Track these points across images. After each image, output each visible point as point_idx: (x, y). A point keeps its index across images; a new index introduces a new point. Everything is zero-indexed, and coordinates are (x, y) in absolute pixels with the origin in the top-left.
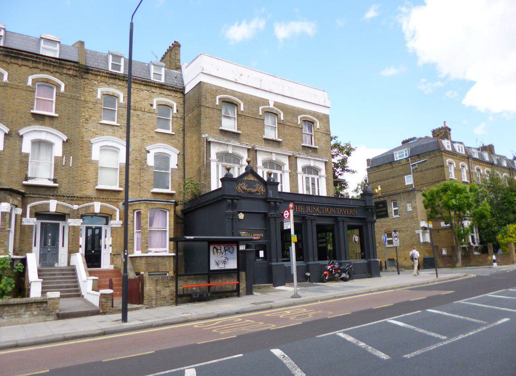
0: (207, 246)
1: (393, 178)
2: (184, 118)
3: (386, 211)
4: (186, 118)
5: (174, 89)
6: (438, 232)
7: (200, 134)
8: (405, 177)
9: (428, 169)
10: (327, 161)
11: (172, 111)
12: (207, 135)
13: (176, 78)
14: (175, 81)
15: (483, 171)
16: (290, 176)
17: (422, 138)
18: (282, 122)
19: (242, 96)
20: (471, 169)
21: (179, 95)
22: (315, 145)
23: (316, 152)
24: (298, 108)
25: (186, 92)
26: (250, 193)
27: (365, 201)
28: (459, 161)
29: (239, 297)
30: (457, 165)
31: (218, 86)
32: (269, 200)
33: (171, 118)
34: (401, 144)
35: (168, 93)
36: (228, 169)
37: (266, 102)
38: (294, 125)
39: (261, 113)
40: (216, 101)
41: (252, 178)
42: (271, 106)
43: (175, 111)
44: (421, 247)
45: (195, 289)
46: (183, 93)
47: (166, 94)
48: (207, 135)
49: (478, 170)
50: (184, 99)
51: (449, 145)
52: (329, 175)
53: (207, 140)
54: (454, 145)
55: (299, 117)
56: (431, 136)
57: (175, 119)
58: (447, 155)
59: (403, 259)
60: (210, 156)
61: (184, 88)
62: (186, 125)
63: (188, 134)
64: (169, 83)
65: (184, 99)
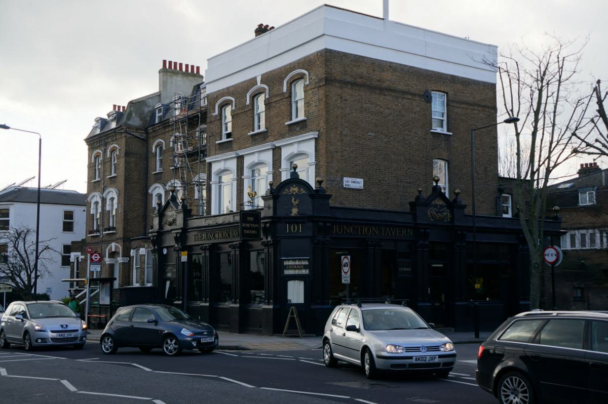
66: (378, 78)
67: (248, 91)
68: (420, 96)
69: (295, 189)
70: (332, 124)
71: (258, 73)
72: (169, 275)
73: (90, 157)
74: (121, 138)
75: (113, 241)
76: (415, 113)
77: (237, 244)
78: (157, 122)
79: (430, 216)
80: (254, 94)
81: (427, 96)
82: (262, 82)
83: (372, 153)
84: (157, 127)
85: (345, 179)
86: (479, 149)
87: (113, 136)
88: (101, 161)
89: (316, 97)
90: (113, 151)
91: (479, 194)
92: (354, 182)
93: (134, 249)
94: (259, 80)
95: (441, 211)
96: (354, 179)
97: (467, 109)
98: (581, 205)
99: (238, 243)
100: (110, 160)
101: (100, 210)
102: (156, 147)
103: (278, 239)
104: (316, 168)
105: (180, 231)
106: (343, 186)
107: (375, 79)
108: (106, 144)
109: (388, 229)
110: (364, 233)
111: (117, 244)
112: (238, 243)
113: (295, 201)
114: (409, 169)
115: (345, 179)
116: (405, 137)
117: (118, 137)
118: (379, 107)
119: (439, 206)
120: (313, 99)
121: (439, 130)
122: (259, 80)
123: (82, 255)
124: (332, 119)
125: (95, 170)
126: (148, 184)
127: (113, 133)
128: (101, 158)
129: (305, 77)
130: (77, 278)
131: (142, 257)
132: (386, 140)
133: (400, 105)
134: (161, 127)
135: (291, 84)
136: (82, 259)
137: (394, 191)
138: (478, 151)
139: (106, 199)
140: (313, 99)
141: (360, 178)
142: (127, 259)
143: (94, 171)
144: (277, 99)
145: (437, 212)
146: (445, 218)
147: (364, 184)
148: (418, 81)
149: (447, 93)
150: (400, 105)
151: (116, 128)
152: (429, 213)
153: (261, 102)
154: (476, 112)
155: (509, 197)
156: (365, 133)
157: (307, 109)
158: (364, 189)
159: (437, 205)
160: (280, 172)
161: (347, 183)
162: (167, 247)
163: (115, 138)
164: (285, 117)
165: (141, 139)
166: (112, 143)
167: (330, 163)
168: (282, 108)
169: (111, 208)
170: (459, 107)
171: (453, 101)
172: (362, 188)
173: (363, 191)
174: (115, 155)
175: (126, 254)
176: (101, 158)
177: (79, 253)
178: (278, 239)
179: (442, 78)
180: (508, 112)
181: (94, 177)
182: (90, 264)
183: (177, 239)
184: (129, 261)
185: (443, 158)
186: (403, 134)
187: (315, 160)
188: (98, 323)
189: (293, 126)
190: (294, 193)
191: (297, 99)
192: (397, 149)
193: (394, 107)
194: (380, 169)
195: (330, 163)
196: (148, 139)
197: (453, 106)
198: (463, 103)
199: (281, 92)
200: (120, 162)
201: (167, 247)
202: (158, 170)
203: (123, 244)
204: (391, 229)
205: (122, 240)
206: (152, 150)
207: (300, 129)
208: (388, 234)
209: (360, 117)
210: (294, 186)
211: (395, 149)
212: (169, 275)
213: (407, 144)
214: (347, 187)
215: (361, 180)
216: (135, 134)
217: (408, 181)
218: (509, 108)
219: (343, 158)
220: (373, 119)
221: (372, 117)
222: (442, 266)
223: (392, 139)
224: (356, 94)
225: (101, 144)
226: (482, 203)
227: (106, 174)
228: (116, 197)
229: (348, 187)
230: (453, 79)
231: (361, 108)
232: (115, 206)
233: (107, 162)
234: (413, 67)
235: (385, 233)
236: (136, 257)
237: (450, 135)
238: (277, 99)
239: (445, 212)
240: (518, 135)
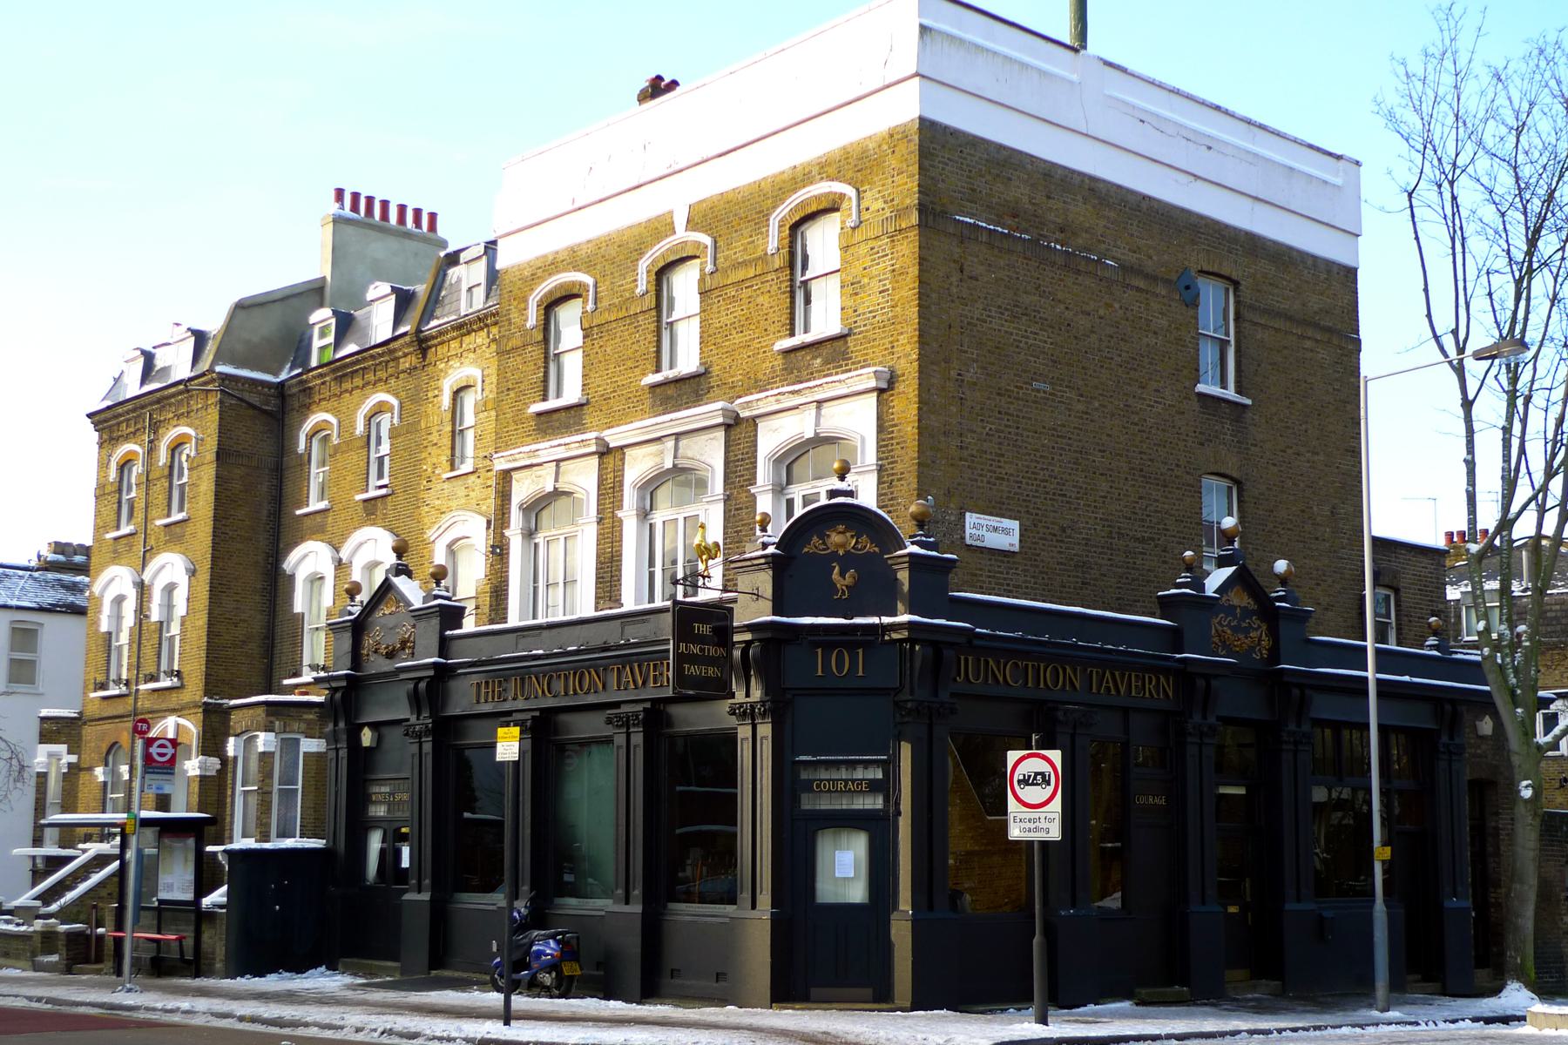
66: (1059, 221)
67: (642, 254)
68: (1168, 282)
69: (838, 538)
70: (935, 345)
71: (677, 199)
72: (379, 811)
73: (103, 465)
74: (206, 407)
75: (173, 711)
76: (1155, 333)
77: (636, 714)
78: (314, 363)
79: (1216, 640)
80: (661, 264)
81: (1187, 288)
82: (691, 224)
83: (1043, 446)
84: (314, 377)
85: (971, 518)
86: (1317, 454)
87: (180, 403)
88: (139, 475)
89: (886, 264)
90: (175, 448)
91: (1318, 584)
92: (996, 529)
93: (237, 735)
94: (680, 221)
95: (1244, 625)
96: (993, 521)
97: (1286, 332)
98: (1467, 639)
99: (640, 707)
100: (166, 472)
101: (129, 620)
102: (310, 438)
103: (789, 696)
104: (880, 482)
105: (431, 673)
106: (963, 538)
107: (1054, 223)
108: (155, 427)
109: (1108, 674)
110: (1042, 686)
111: (182, 721)
112: (640, 707)
113: (842, 574)
114: (1141, 498)
115: (971, 518)
116: (1131, 401)
117: (196, 404)
118: (1062, 306)
119: (1238, 610)
120: (874, 271)
121: (1216, 390)
122: (680, 221)
123: (69, 752)
124: (934, 332)
125: (120, 502)
126: (281, 546)
127: (180, 393)
128: (137, 469)
129: (845, 206)
130: (65, 810)
131: (1383, 611)
132: (1081, 407)
133: (1117, 306)
134: (327, 378)
135: (795, 227)
136: (69, 764)
137: (1100, 561)
138: (1316, 458)
139: (150, 587)
140: (874, 271)
141: (1010, 518)
142: (214, 762)
143: (115, 506)
144: (741, 274)
145: (1235, 629)
146: (1254, 648)
147: (1021, 535)
148: (1162, 240)
149: (1236, 284)
150: (1117, 306)
151: (191, 379)
152: (1213, 631)
153: (685, 284)
154: (1308, 344)
155: (1389, 596)
156: (1026, 383)
157: (850, 303)
158: (1020, 552)
159: (1235, 607)
160: (754, 497)
161: (974, 531)
162: (375, 726)
163: (184, 410)
164: (771, 329)
165: (265, 412)
166: (175, 423)
167: (928, 466)
168: (760, 300)
169: (115, 624)
170: (1264, 327)
171: (1252, 308)
172: (1016, 548)
173: (1018, 559)
174: (184, 458)
175: (212, 743)
176: (137, 469)
177: (63, 748)
178: (789, 696)
179: (1224, 236)
180: (1436, 337)
181: (114, 524)
182: (145, 772)
183: (415, 701)
184: (222, 772)
185: (1228, 472)
186: (1125, 394)
187: (879, 459)
188: (152, 959)
189: (800, 354)
190: (841, 552)
191: (808, 275)
192: (1108, 435)
193: (1101, 312)
194: (1065, 495)
195: (928, 466)
196: (284, 413)
197: (1251, 321)
198: (1279, 314)
199: (759, 253)
200: (199, 478)
201: (375, 726)
202: (315, 505)
203: (204, 721)
204: (1117, 673)
205: (201, 710)
206: (297, 444)
207: (826, 362)
208: (1108, 689)
209: (1012, 334)
210: (841, 528)
211: (1104, 437)
212: (379, 811)
213: (1136, 424)
214: (974, 543)
215: (1014, 525)
216: (246, 396)
217: (1139, 535)
218: (1444, 323)
219: (966, 453)
220: (1045, 342)
221: (1043, 335)
222: (1241, 791)
223: (1097, 404)
224: (1002, 263)
225: (138, 426)
226: (1327, 609)
227: (153, 513)
228: (183, 581)
229: (979, 543)
230: (1253, 245)
231: (1015, 306)
232: (180, 608)
233: (158, 479)
234: (1150, 198)
235: (1099, 690)
236: (246, 759)
237: (1245, 406)
238: (741, 274)
239: (1257, 629)
240: (1467, 405)
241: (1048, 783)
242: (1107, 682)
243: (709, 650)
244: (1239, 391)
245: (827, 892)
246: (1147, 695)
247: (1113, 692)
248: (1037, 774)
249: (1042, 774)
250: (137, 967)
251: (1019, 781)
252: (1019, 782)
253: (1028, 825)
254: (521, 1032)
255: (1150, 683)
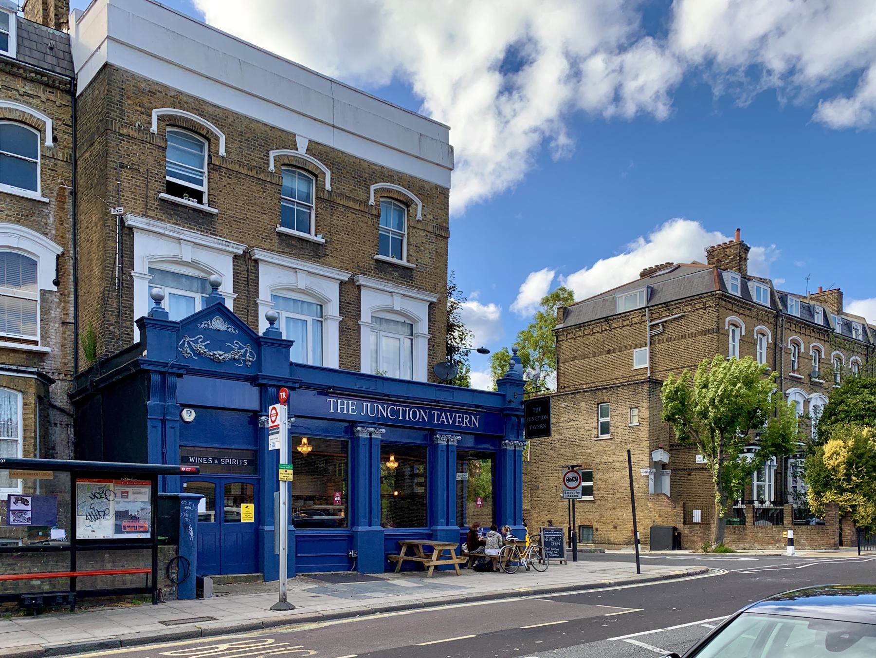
0: (68, 484)
1: (609, 352)
2: (76, 161)
3: (548, 422)
4: (80, 163)
5: (45, 79)
6: (690, 475)
7: (106, 206)
8: (635, 350)
9: (683, 337)
10: (435, 300)
11: (43, 140)
12: (121, 210)
13: (51, 49)
14: (49, 59)
15: (806, 348)
16: (341, 331)
17: (685, 265)
18: (326, 196)
19: (223, 118)
20: (778, 341)
21: (60, 99)
22: (408, 261)
23: (411, 278)
24: (370, 164)
25: (81, 86)
26: (213, 360)
27: (504, 396)
28: (754, 321)
29: (155, 602)
30: (750, 332)
31: (157, 84)
32: (261, 381)
33: (39, 161)
34: (639, 278)
35: (28, 88)
36: (158, 300)
37: (288, 140)
38: (357, 207)
39: (272, 167)
40: (150, 123)
41: (218, 324)
42: (302, 150)
43: (49, 142)
44: (650, 505)
45: (36, 583)
46: (72, 92)
47: (22, 91)
48: (121, 210)
49: (797, 344)
50: (75, 110)
51: (735, 282)
52: (437, 334)
53: (122, 221)
54: (751, 285)
55: (373, 188)
56: (705, 261)
57: (51, 163)
58: (729, 306)
59: (611, 527)
60: (132, 266)
61: (73, 81)
62: (81, 181)
63: (83, 206)
64: (29, 60)
65: (75, 110)
109: (443, 414)
241: (577, 480)
242: (443, 418)
243: (404, 412)
244: (43, 195)
245: (252, 506)
246: (464, 425)
247: (446, 423)
248: (573, 477)
249: (575, 477)
250: (201, 152)
251: (567, 480)
252: (567, 480)
253: (570, 495)
254: (51, 639)
255: (466, 419)
